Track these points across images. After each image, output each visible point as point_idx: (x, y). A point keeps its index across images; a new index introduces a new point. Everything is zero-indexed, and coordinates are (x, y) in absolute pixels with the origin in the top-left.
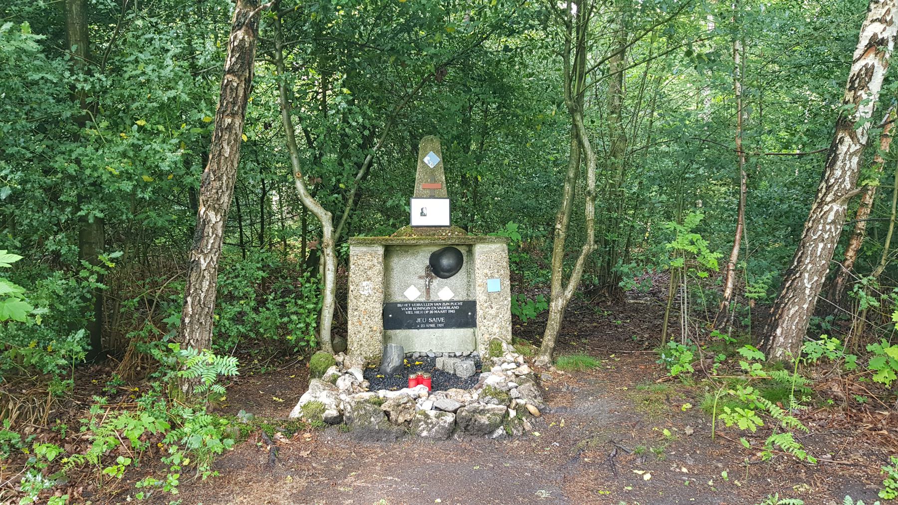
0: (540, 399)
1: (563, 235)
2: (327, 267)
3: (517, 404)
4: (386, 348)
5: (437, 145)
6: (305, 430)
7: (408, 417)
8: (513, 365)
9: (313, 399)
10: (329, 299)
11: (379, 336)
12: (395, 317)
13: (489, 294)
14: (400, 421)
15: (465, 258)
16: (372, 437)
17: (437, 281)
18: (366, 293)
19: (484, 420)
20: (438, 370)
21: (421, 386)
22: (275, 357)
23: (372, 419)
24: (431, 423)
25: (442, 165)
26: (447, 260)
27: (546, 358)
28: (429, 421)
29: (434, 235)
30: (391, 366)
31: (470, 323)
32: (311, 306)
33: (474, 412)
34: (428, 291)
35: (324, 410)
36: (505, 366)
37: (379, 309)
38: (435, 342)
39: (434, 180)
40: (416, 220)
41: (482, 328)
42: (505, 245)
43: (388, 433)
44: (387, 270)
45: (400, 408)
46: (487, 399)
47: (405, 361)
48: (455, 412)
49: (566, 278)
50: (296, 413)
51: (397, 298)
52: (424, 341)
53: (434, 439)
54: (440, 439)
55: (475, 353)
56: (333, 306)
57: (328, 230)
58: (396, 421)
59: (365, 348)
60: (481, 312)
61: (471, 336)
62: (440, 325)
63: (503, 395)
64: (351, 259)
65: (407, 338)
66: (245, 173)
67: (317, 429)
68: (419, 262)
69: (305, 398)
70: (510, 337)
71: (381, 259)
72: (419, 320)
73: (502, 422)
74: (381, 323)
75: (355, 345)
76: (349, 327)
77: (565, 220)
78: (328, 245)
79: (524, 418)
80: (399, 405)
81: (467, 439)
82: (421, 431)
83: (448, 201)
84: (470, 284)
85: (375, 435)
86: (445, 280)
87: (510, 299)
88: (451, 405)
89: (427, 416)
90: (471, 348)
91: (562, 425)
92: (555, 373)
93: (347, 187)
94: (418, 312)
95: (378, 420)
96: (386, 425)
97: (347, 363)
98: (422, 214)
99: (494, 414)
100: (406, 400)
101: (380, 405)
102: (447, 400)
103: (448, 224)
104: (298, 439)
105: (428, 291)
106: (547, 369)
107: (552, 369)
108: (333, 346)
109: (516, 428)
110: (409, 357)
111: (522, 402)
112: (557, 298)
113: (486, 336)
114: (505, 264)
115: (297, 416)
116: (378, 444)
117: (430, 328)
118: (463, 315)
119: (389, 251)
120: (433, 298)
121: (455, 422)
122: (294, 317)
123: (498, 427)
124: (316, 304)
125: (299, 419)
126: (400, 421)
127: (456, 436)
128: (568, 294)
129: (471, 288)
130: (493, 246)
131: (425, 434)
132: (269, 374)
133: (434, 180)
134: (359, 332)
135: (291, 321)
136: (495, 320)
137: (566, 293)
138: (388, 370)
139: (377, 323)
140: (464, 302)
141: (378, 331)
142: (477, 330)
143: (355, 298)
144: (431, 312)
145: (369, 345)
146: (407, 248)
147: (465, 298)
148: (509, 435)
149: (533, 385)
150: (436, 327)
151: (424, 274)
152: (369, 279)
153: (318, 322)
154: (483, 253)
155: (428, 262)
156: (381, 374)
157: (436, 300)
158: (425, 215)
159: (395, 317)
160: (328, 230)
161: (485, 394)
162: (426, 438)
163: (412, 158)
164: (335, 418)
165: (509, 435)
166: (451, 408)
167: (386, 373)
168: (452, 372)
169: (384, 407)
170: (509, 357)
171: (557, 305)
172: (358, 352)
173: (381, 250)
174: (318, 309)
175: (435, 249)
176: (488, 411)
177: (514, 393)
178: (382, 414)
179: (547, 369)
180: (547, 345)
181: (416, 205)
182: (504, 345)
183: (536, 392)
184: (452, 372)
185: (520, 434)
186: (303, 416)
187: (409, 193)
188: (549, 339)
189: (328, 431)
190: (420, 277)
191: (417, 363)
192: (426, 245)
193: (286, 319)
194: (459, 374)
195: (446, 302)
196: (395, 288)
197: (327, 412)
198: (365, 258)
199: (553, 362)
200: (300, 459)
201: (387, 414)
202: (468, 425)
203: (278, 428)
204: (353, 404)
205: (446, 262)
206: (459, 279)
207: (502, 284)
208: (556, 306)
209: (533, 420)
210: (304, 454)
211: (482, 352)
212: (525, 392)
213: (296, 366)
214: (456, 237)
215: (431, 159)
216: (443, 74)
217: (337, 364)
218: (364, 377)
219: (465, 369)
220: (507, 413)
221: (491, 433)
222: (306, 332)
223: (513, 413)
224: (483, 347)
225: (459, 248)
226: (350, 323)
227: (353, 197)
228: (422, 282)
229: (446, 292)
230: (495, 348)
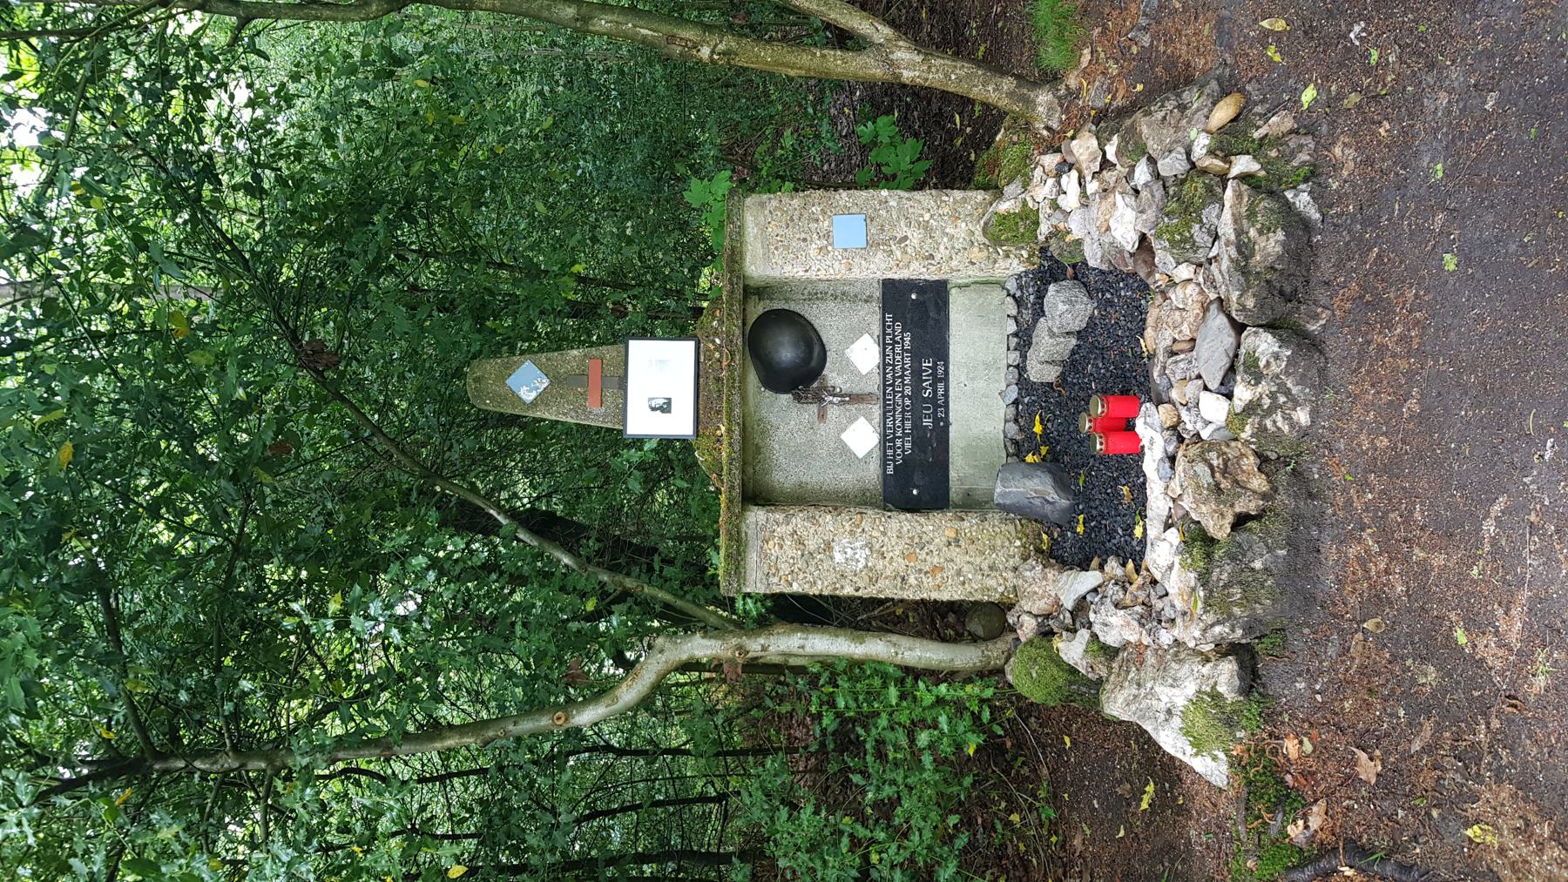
0: (1191, 96)
1: (727, 43)
2: (795, 651)
3: (1211, 152)
4: (1003, 508)
5: (489, 367)
6: (1275, 752)
7: (1250, 462)
8: (1070, 181)
9: (1177, 722)
10: (875, 648)
11: (970, 523)
12: (917, 479)
13: (872, 244)
14: (1265, 488)
15: (777, 305)
16: (1306, 566)
17: (833, 376)
18: (862, 555)
19: (1271, 245)
20: (1063, 376)
21: (1139, 422)
22: (1007, 772)
23: (1258, 565)
24: (1273, 396)
25: (543, 357)
26: (777, 348)
27: (1043, 98)
28: (1266, 402)
29: (718, 380)
30: (1052, 495)
31: (936, 294)
32: (893, 693)
33: (1245, 272)
34: (856, 398)
35: (1216, 696)
36: (1070, 200)
37: (902, 523)
38: (982, 384)
39: (581, 377)
40: (680, 424)
41: (954, 263)
42: (749, 201)
43: (1296, 519)
44: (804, 499)
45: (1225, 484)
46: (1200, 237)
47: (1029, 458)
48: (1239, 328)
49: (843, 39)
50: (1212, 768)
51: (872, 474)
52: (979, 408)
53: (1320, 389)
54: (1322, 372)
55: (1012, 286)
56: (894, 638)
57: (701, 647)
58: (1264, 496)
59: (999, 558)
60: (915, 265)
61: (970, 294)
62: (940, 370)
63: (1185, 198)
64: (777, 590)
65: (970, 451)
66: (553, 850)
67: (1270, 717)
68: (784, 416)
69: (1171, 741)
70: (979, 196)
71: (780, 516)
72: (927, 422)
73: (1271, 193)
74: (937, 517)
75: (991, 583)
76: (945, 596)
77: (689, 34)
78: (740, 648)
79: (1256, 135)
80: (1218, 489)
81: (1321, 295)
82: (1292, 425)
83: (633, 344)
84: (842, 294)
85: (1302, 555)
86: (831, 356)
87: (884, 193)
88: (1216, 340)
89: (1251, 408)
90: (997, 295)
91: (1280, 25)
92: (1086, 73)
93: (593, 592)
94: (908, 424)
95: (1259, 547)
96: (1276, 526)
97: (1040, 606)
98: (666, 408)
99: (1251, 215)
100: (1201, 469)
101: (1209, 541)
102: (1203, 348)
103: (691, 344)
104: (1308, 775)
105: (856, 398)
106: (1074, 95)
107: (1072, 82)
108: (992, 636)
109: (1293, 154)
110: (1018, 449)
111: (1201, 143)
112: (892, 64)
113: (975, 254)
114: (796, 202)
115: (1224, 768)
116: (1330, 553)
117: (946, 395)
118: (917, 311)
119: (756, 495)
120: (873, 385)
121: (1271, 327)
122: (923, 738)
123: (1288, 207)
124: (885, 678)
125: (1236, 763)
126: (1265, 488)
127: (1313, 327)
128: (878, 31)
129: (852, 291)
130: (751, 230)
131: (1302, 416)
132: (1055, 796)
133: (581, 377)
134: (959, 573)
135: (932, 746)
136: (935, 233)
137: (878, 39)
138: (1064, 503)
139: (936, 527)
140: (885, 310)
141: (957, 524)
142: (955, 279)
143: (873, 581)
144: (908, 391)
145: (993, 548)
146: (750, 447)
147: (875, 307)
148: (1313, 174)
149: (1148, 113)
150: (946, 379)
151: (814, 408)
152: (828, 547)
153: (935, 675)
154: (767, 257)
155: (785, 398)
156: (1075, 521)
157: (877, 380)
158: (669, 402)
159: (917, 479)
160: (701, 647)
161: (1183, 246)
162: (1314, 414)
163: (527, 432)
164: (1242, 666)
165: (1313, 174)
166: (1228, 339)
167: (1073, 511)
168: (1074, 341)
169: (1219, 528)
170: (1042, 191)
171: (911, 65)
172: (1010, 575)
173: (757, 516)
174: (899, 674)
175: (753, 378)
176: (1239, 232)
177: (1172, 165)
178: (1241, 537)
179: (1074, 95)
180: (1010, 94)
181: (641, 422)
182: (1004, 207)
183: (1170, 105)
184: (1074, 341)
185: (1309, 141)
186: (1227, 752)
187: (615, 439)
188: (994, 91)
189: (1275, 687)
190: (822, 416)
191: (1038, 429)
192: (744, 398)
193: (927, 759)
194: (1079, 324)
195: (884, 355)
196: (847, 479)
197: (1222, 689)
198: (781, 554)
199: (1051, 78)
200: (1388, 783)
201: (1240, 521)
202: (1281, 293)
203: (1273, 833)
204: (1210, 618)
205: (786, 352)
206: (827, 321)
207: (847, 211)
208: (911, 66)
209: (1259, 109)
210: (1368, 769)
211: (1012, 266)
212: (1168, 135)
213: (1035, 726)
214: (725, 328)
215: (527, 383)
216: (318, 349)
217: (1047, 634)
218: (1084, 566)
219: (1066, 309)
220: (1245, 178)
221: (1306, 224)
222: (959, 707)
223: (1243, 164)
224: (1002, 264)
225: (751, 320)
226: (935, 596)
227: (619, 578)
228: (833, 412)
229: (859, 355)
230: (1002, 232)
